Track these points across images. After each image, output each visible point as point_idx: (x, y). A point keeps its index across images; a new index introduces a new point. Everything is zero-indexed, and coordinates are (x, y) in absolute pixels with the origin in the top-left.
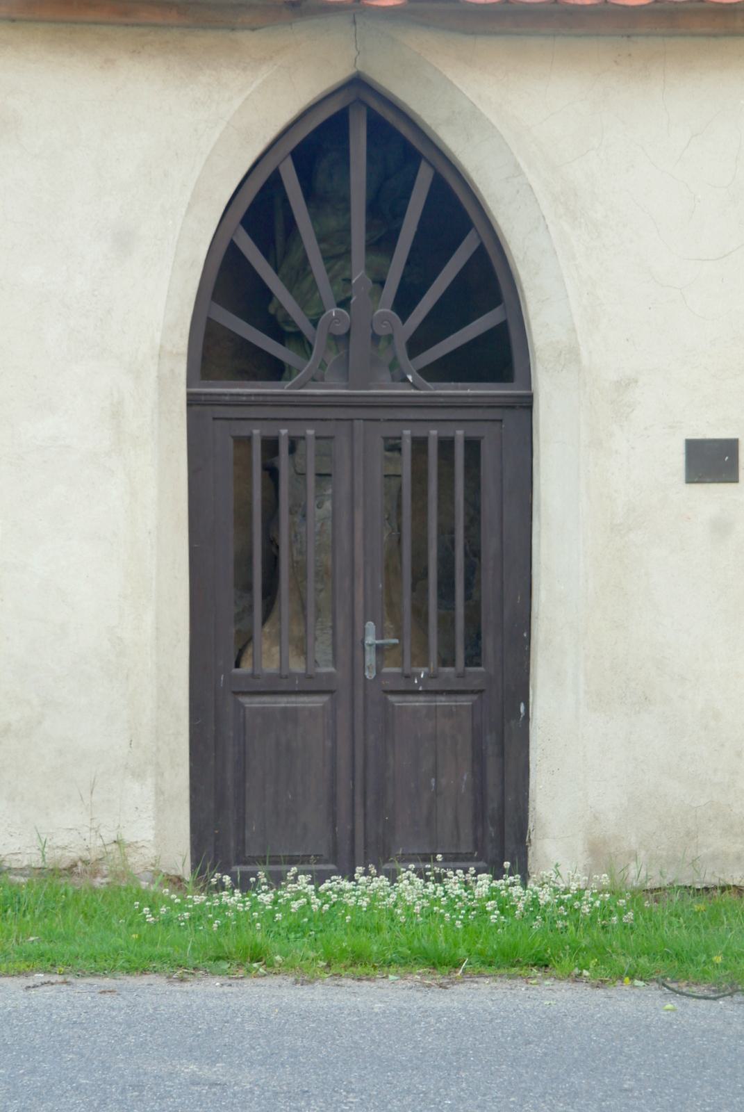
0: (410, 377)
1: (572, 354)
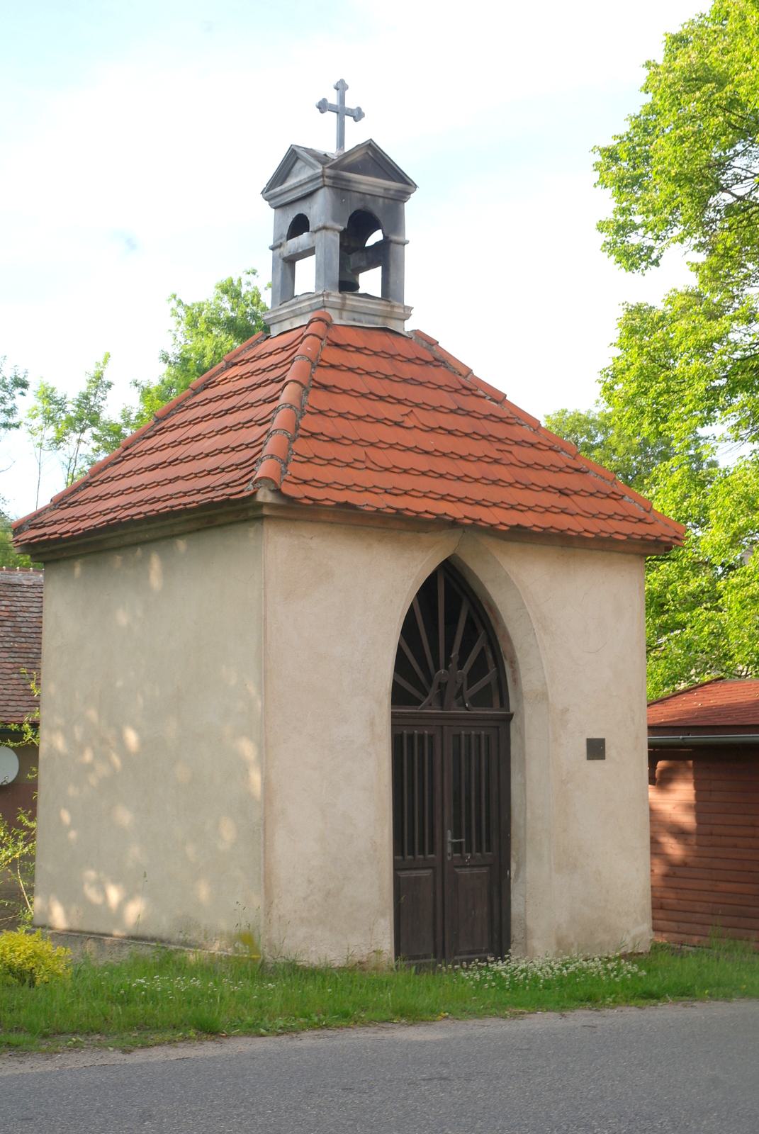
0: (467, 705)
1: (543, 696)
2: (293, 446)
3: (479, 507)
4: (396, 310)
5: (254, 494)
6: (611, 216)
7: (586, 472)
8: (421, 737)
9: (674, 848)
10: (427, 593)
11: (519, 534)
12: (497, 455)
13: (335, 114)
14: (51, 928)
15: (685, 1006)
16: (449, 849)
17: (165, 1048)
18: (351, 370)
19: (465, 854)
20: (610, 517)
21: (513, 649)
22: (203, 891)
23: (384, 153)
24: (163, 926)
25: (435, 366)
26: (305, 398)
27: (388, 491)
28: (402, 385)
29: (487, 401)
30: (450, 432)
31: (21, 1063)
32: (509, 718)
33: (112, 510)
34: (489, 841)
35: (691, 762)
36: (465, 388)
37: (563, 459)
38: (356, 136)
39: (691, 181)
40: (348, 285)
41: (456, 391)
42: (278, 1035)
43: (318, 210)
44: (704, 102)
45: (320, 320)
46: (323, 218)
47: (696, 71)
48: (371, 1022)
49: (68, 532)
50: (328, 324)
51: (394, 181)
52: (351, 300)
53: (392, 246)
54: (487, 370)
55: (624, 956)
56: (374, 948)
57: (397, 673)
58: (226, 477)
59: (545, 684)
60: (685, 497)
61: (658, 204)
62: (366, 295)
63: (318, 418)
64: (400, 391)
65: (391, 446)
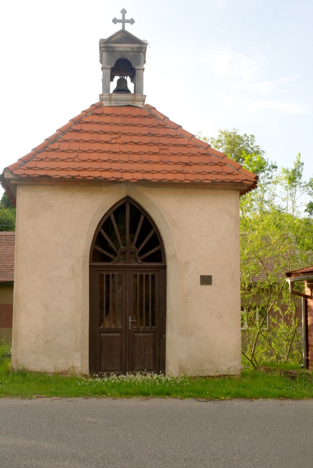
0: (139, 261)
7: (210, 155)
16: (130, 324)
23: (130, 33)
27: (75, 169)
37: (202, 150)
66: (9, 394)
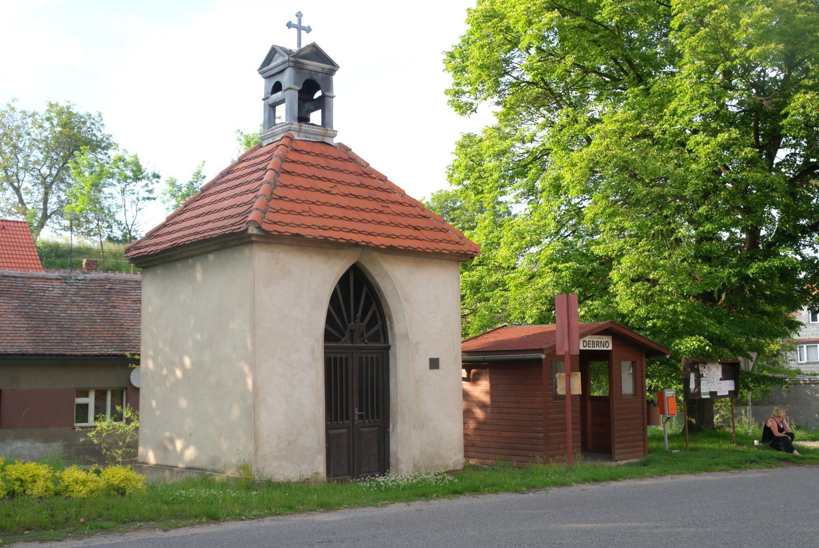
1: (406, 336)
2: (269, 204)
3: (371, 236)
4: (329, 132)
5: (247, 230)
6: (451, 87)
8: (341, 359)
9: (479, 413)
10: (344, 282)
11: (392, 251)
12: (381, 209)
13: (296, 29)
14: (147, 464)
15: (473, 497)
16: (356, 418)
17: (187, 528)
18: (303, 163)
19: (365, 420)
20: (441, 241)
21: (390, 311)
22: (225, 445)
24: (203, 462)
25: (350, 162)
26: (277, 178)
28: (331, 172)
29: (377, 180)
30: (356, 197)
31: (105, 538)
32: (388, 348)
33: (175, 239)
34: (378, 414)
35: (488, 370)
36: (365, 173)
38: (307, 40)
39: (488, 68)
40: (303, 119)
41: (361, 175)
42: (252, 519)
43: (286, 79)
44: (493, 27)
45: (287, 137)
46: (289, 83)
47: (489, 12)
48: (305, 511)
49: (152, 251)
50: (291, 139)
51: (327, 64)
52: (305, 127)
53: (327, 98)
54: (377, 164)
55: (447, 472)
56: (315, 471)
57: (580, 358)
58: (233, 221)
59: (407, 330)
60: (490, 232)
61: (473, 80)
62: (313, 124)
63: (284, 189)
64: (329, 174)
65: (324, 204)
66: (306, 502)
